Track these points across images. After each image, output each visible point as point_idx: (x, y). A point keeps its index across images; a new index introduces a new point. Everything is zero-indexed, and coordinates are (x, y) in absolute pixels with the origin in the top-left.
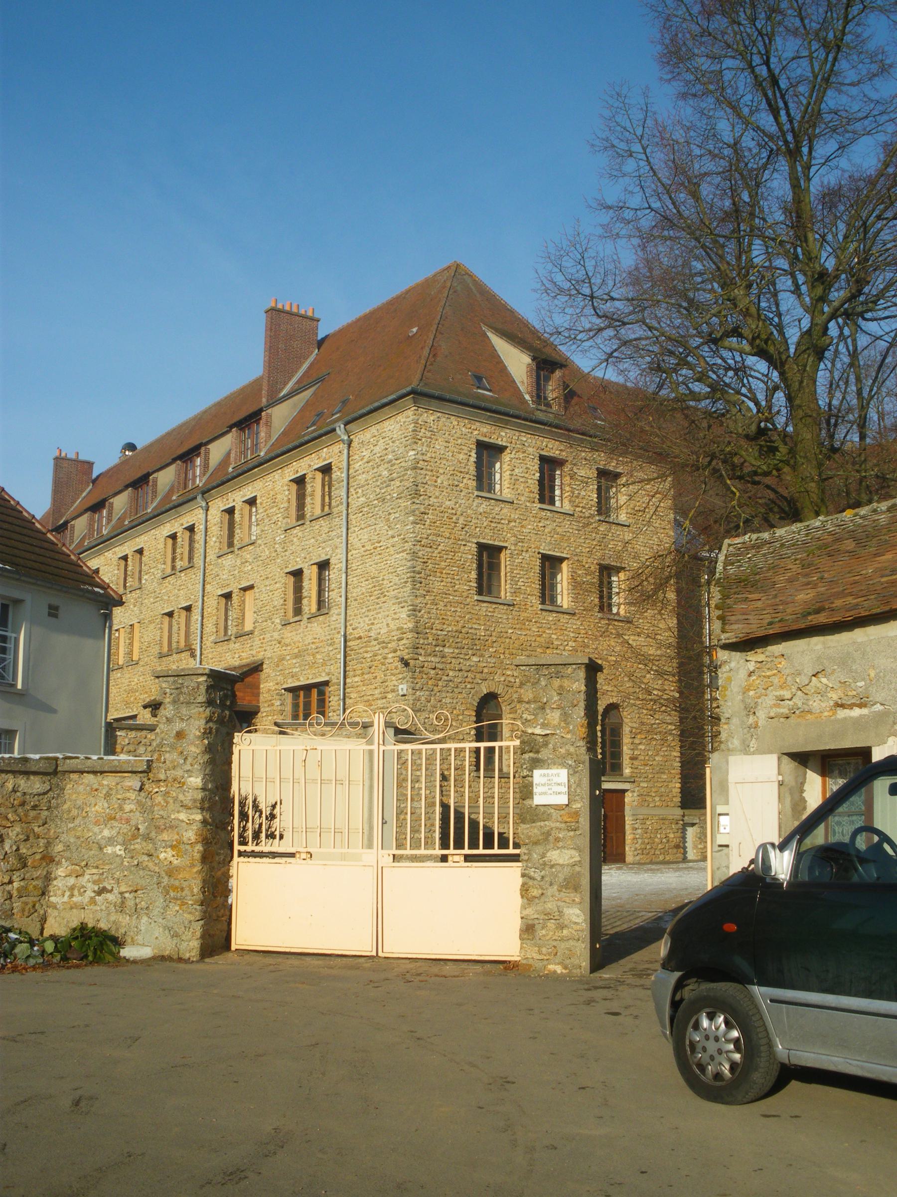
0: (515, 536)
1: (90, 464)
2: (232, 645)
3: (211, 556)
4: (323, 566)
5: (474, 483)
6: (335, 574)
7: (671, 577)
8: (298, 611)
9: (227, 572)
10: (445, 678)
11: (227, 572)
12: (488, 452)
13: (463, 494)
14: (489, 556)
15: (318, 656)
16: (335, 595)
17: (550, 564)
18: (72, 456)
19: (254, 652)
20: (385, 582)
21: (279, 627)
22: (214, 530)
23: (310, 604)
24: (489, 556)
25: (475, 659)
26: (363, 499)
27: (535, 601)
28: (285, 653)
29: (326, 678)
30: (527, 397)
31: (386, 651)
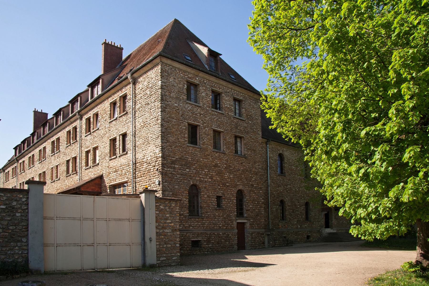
0: (202, 120)
1: (46, 114)
2: (91, 170)
3: (83, 137)
4: (124, 136)
5: (186, 98)
6: (129, 138)
7: (427, 9)
8: (115, 154)
9: (88, 142)
10: (176, 178)
11: (88, 142)
12: (192, 86)
13: (181, 101)
14: (193, 130)
15: (123, 171)
16: (129, 146)
17: (217, 133)
18: (40, 111)
19: (99, 172)
20: (149, 138)
21: (108, 161)
22: (84, 127)
23: (119, 151)
24: (193, 130)
25: (188, 170)
26: (140, 105)
27: (211, 148)
28: (110, 171)
29: (127, 180)
30: (206, 66)
31: (150, 167)
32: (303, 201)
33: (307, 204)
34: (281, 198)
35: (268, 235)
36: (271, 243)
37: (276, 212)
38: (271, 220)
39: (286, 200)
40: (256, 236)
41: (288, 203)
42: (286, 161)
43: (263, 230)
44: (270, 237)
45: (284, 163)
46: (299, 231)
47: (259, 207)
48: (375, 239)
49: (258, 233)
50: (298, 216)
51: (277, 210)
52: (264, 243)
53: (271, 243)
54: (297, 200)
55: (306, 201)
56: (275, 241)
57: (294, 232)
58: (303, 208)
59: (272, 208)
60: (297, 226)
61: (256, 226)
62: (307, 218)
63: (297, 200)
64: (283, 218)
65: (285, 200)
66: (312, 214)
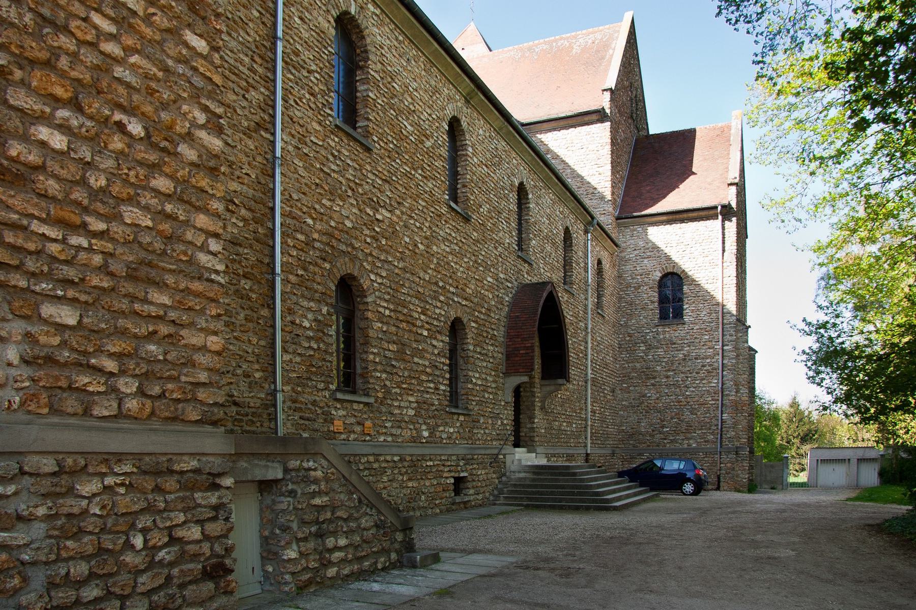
32: (443, 313)
33: (456, 328)
34: (344, 267)
35: (265, 486)
36: (292, 554)
37: (318, 340)
38: (287, 381)
39: (371, 281)
40: (126, 502)
41: (377, 304)
42: (374, 68)
43: (214, 444)
44: (285, 503)
45: (366, 81)
46: (423, 457)
47: (162, 183)
48: (454, 484)
49: (156, 469)
50: (421, 382)
51: (321, 325)
52: (218, 571)
53: (292, 554)
54: (419, 296)
55: (453, 315)
56: (320, 535)
57: (402, 460)
58: (441, 343)
59: (290, 311)
60: (418, 431)
61: (127, 385)
62: (454, 397)
63: (419, 296)
64: (350, 379)
65: (366, 284)
66: (475, 376)
